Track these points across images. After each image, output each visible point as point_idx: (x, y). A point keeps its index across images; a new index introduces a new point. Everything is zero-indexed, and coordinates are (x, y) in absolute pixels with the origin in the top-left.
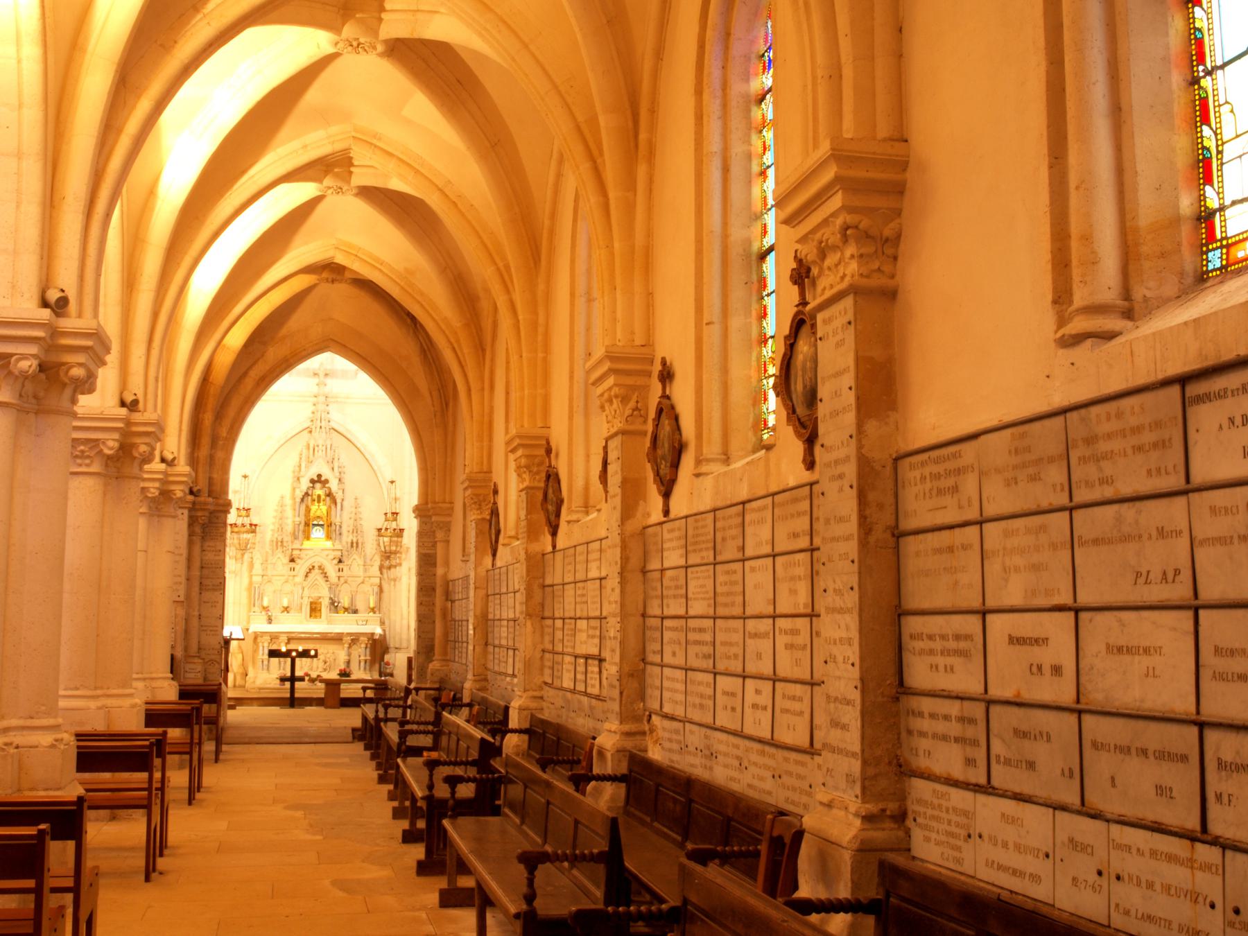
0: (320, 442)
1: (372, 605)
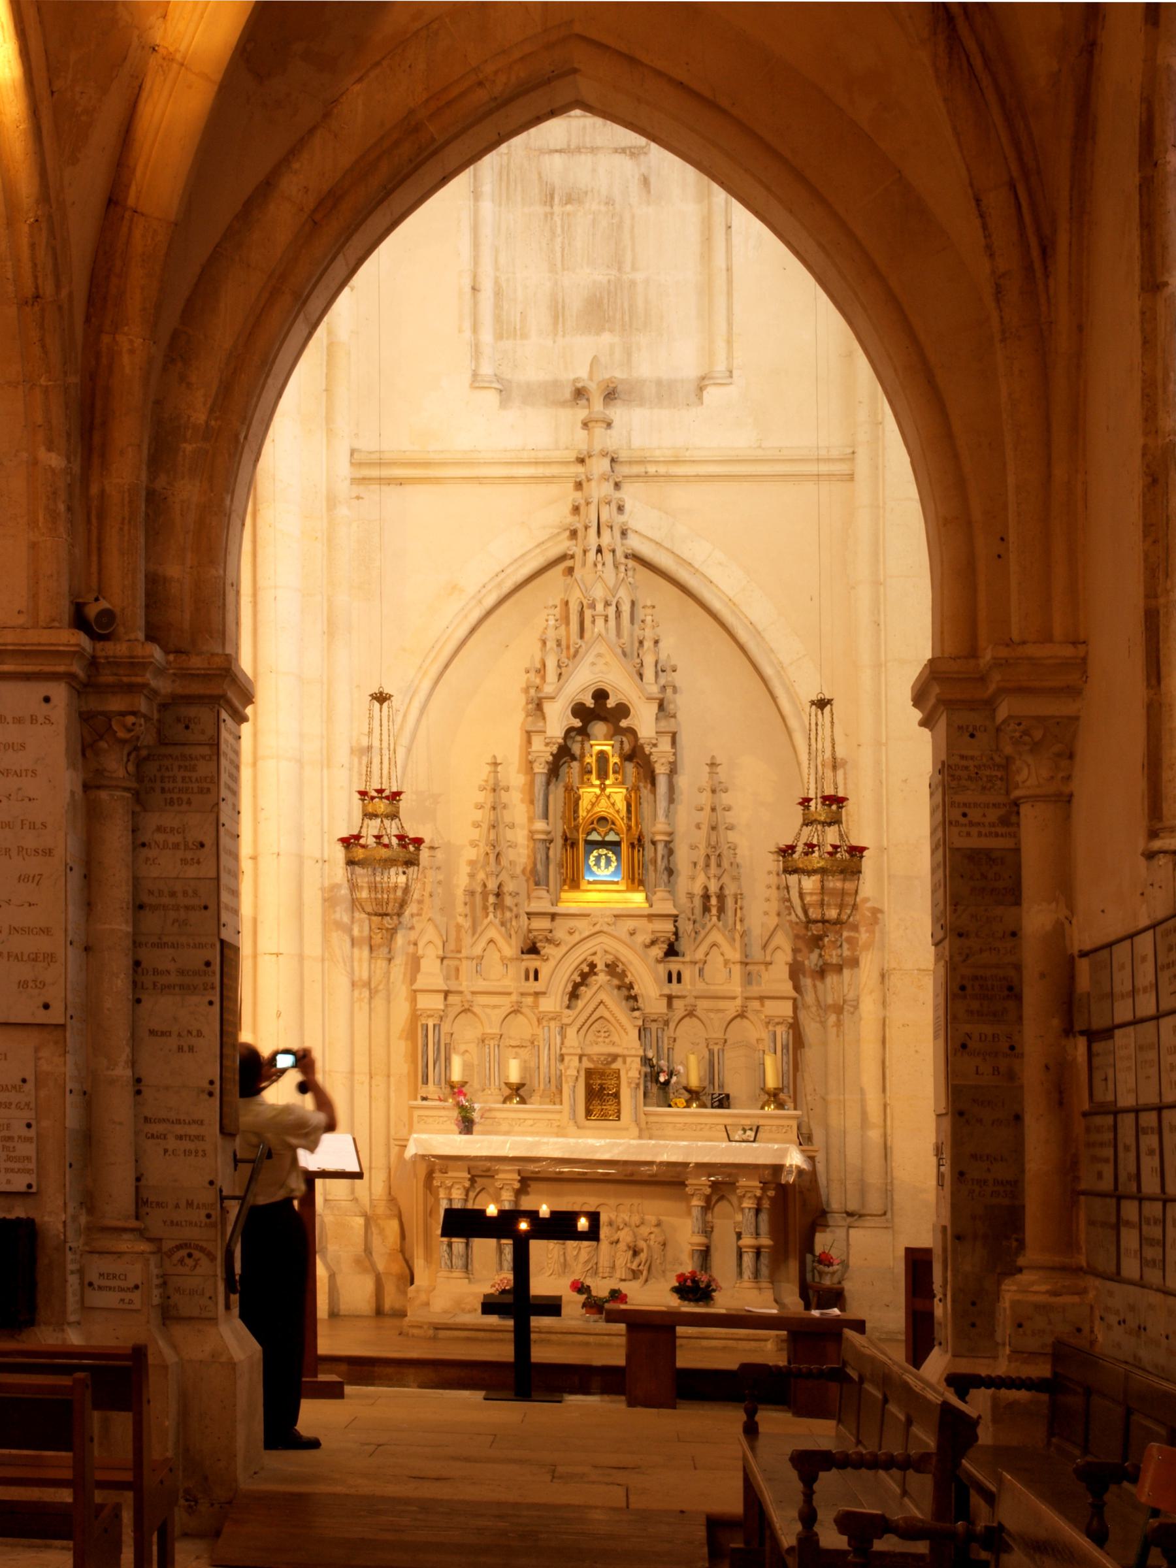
0: (599, 593)
1: (771, 1082)
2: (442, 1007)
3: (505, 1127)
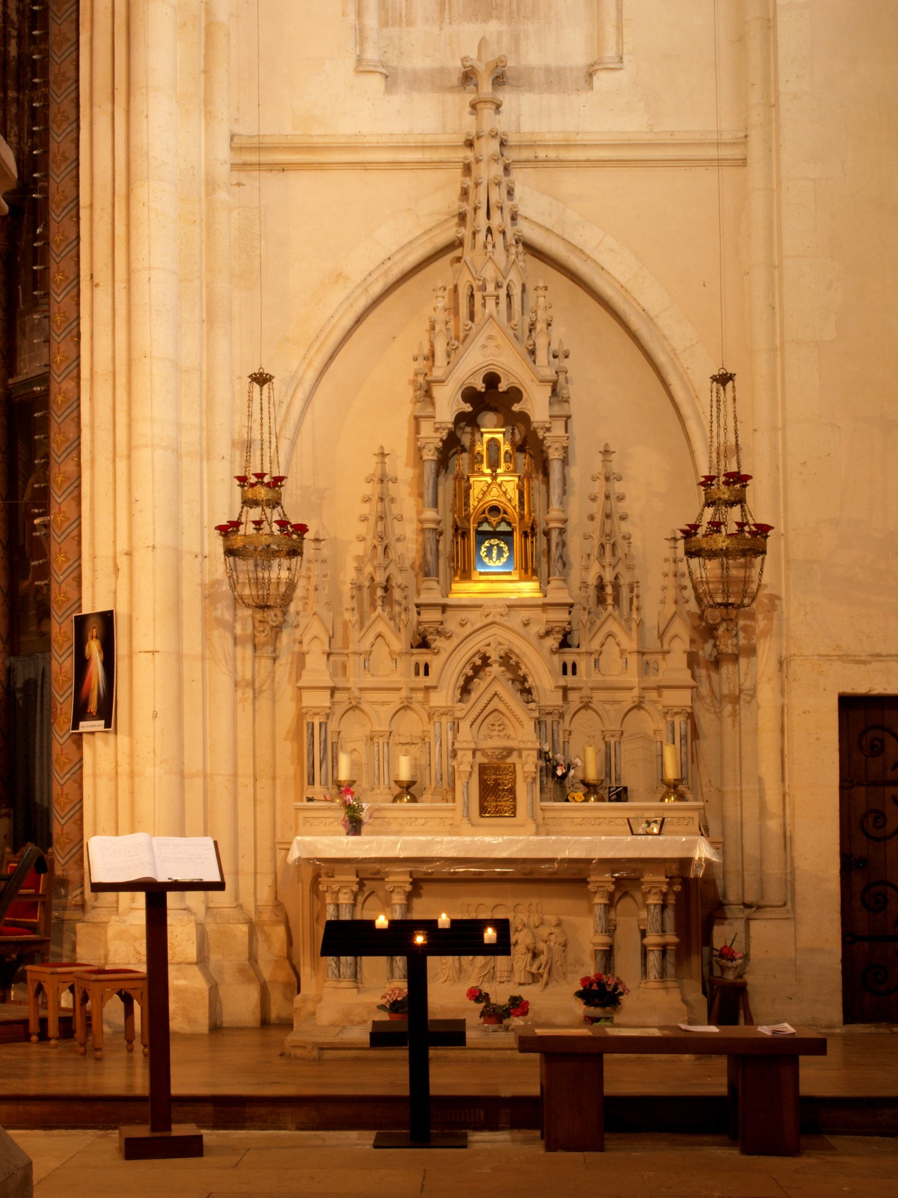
0: (489, 273)
1: (671, 773)
2: (328, 704)
3: (395, 827)
